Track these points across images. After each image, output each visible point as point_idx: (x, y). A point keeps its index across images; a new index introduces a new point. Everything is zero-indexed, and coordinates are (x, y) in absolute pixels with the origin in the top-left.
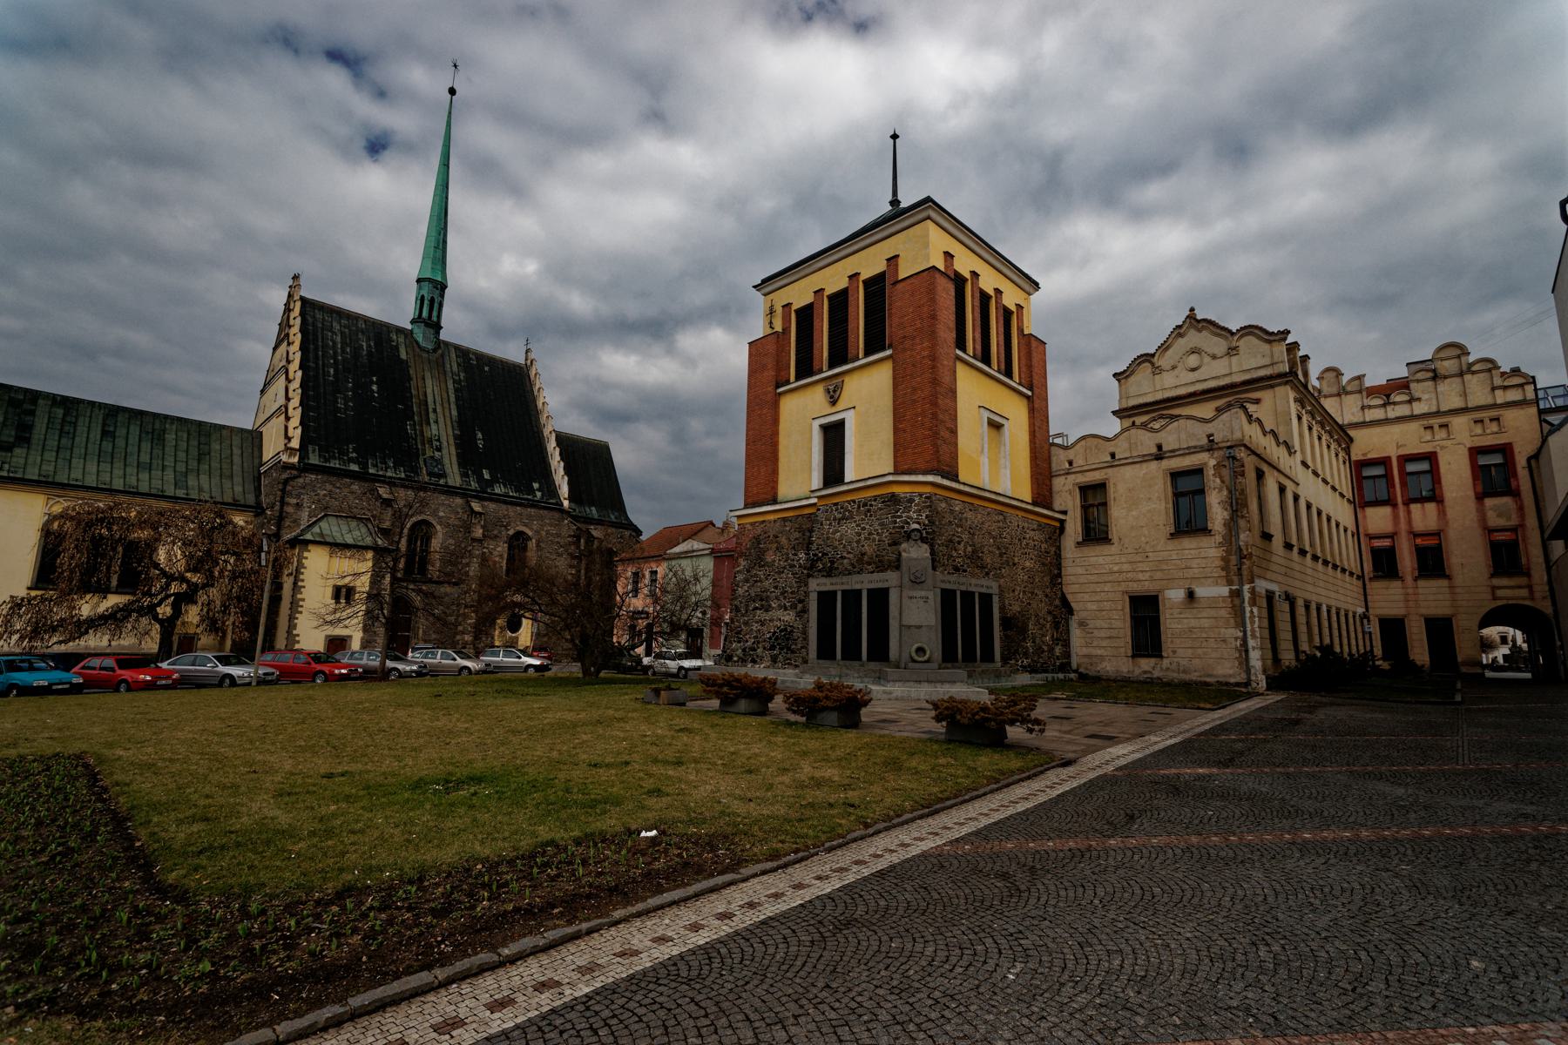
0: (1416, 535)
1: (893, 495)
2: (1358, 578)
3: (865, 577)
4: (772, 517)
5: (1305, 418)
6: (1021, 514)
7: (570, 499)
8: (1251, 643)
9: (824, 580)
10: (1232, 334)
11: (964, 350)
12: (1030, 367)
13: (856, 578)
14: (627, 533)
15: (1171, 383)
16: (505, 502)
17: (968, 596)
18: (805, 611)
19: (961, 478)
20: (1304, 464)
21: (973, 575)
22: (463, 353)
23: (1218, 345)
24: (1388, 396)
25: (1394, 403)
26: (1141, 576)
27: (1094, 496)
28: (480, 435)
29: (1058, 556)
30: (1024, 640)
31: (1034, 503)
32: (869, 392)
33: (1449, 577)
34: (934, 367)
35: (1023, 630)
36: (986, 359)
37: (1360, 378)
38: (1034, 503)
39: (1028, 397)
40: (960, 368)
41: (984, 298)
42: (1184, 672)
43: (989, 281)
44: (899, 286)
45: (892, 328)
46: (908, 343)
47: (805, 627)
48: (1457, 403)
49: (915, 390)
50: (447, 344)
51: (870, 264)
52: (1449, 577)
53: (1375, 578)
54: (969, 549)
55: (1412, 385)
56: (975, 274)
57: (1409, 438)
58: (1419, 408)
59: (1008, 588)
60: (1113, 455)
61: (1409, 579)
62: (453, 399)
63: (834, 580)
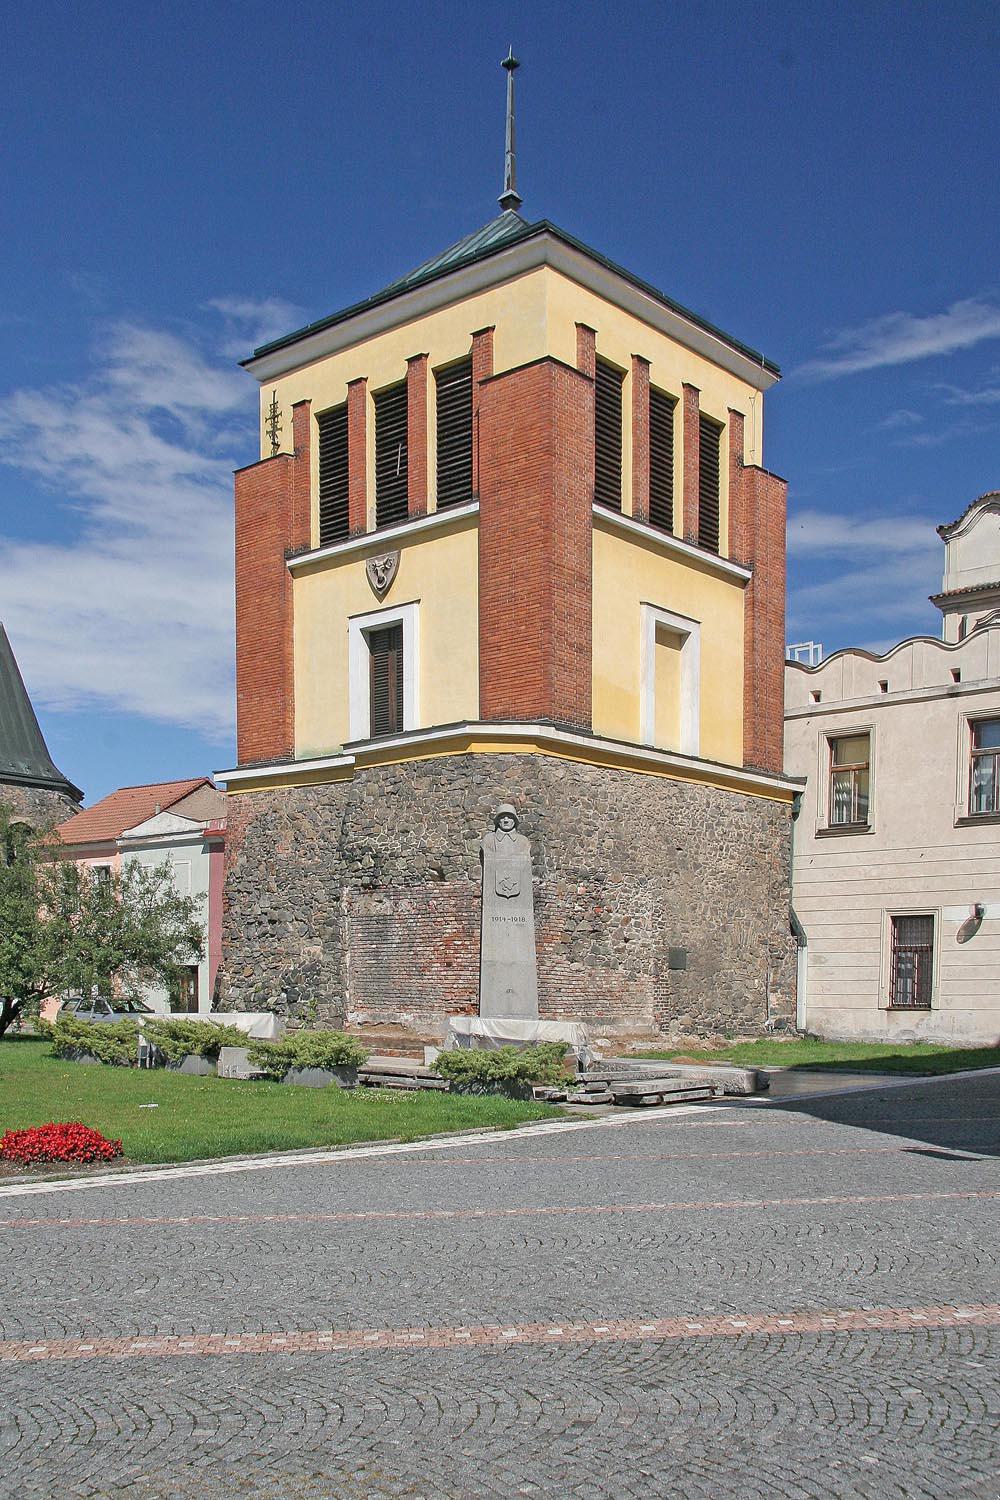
19: (596, 729)
26: (910, 886)
29: (787, 850)
32: (440, 582)
36: (660, 516)
38: (749, 766)
40: (599, 537)
41: (660, 404)
46: (502, 496)
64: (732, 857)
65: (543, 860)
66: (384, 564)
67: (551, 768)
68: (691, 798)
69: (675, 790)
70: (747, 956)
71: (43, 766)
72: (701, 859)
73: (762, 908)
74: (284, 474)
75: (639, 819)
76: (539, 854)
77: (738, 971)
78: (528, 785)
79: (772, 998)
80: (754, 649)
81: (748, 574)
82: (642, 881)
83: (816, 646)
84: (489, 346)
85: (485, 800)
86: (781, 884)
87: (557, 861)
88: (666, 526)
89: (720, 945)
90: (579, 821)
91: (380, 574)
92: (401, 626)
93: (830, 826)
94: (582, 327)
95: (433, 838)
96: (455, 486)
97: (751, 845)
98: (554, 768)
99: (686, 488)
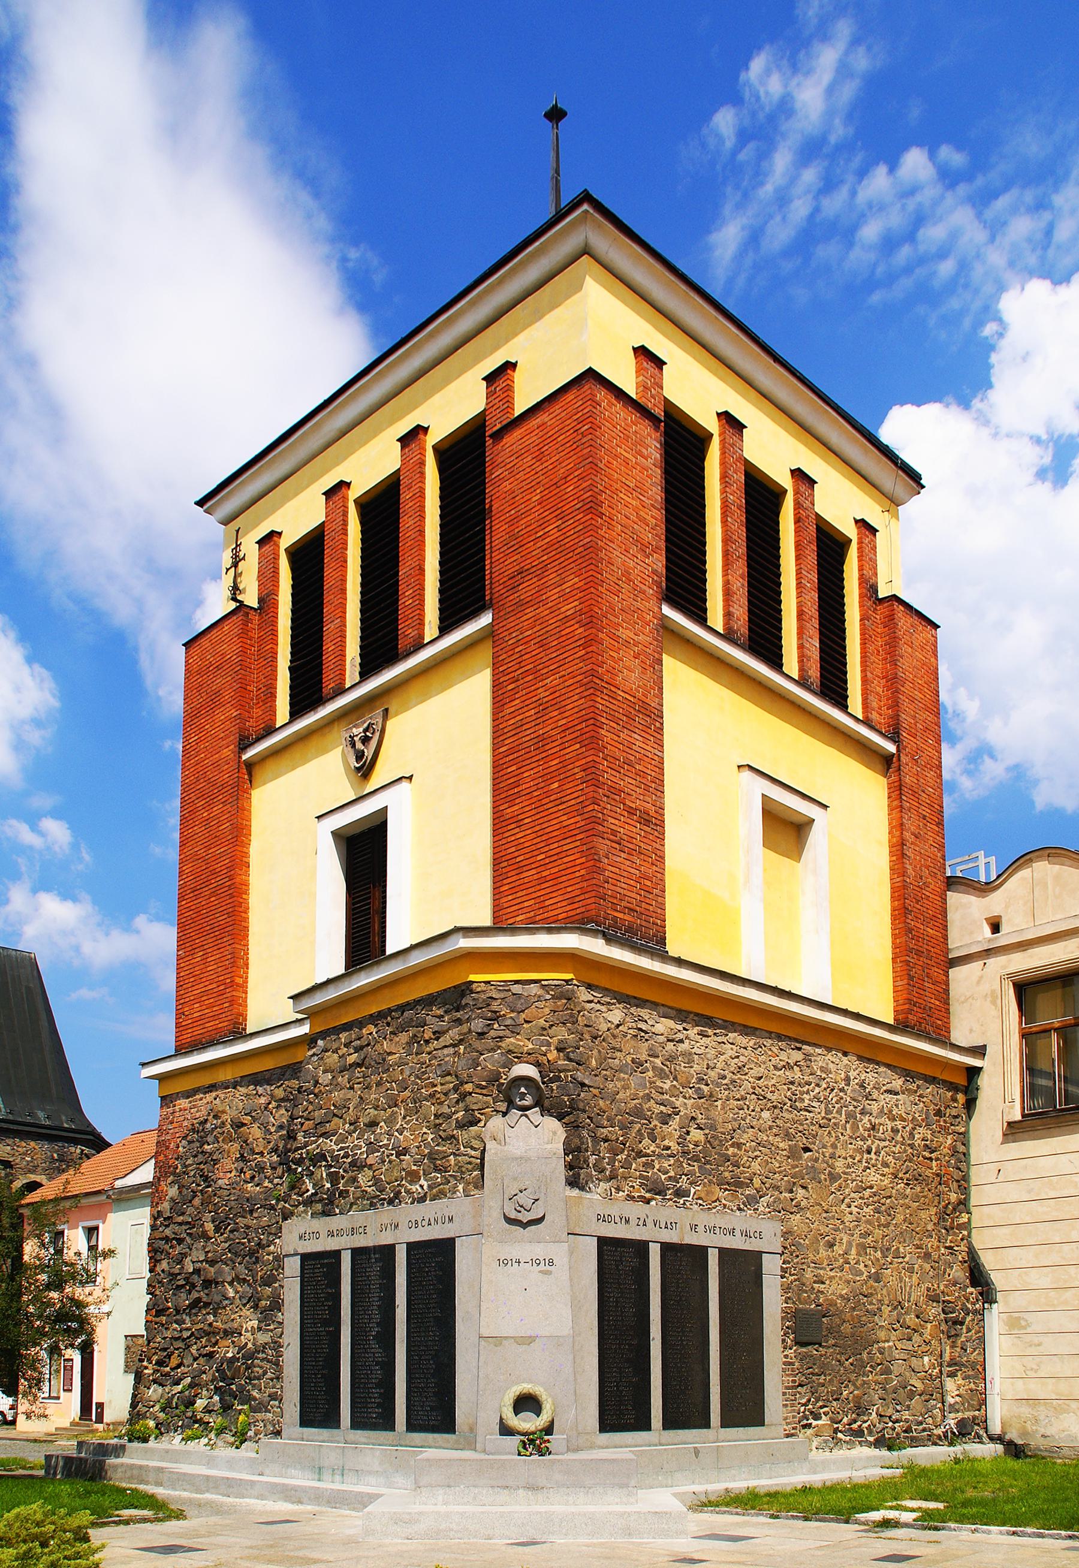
3: (406, 1212)
9: (322, 1224)
12: (893, 681)
13: (386, 1214)
17: (685, 1260)
18: (277, 1305)
21: (708, 1204)
29: (961, 1155)
31: (901, 1026)
32: (440, 750)
34: (590, 641)
35: (859, 1343)
36: (764, 641)
38: (901, 1026)
39: (886, 763)
41: (760, 498)
44: (511, 439)
45: (500, 561)
46: (527, 590)
49: (543, 708)
56: (731, 423)
63: (337, 1222)
64: (886, 1165)
65: (586, 1161)
66: (365, 731)
67: (598, 1006)
68: (822, 1069)
69: (797, 1056)
70: (911, 1319)
71: (67, 1116)
72: (840, 1165)
73: (931, 1243)
74: (244, 632)
75: (744, 1098)
76: (578, 1149)
77: (899, 1345)
78: (561, 1033)
79: (950, 1385)
80: (903, 855)
81: (892, 748)
82: (751, 1201)
83: (987, 860)
85: (490, 1061)
86: (954, 1213)
87: (612, 1162)
89: (871, 1303)
90: (648, 1097)
91: (359, 746)
92: (383, 826)
93: (1023, 1116)
95: (413, 1130)
97: (912, 1146)
98: (604, 1008)
99: (800, 614)
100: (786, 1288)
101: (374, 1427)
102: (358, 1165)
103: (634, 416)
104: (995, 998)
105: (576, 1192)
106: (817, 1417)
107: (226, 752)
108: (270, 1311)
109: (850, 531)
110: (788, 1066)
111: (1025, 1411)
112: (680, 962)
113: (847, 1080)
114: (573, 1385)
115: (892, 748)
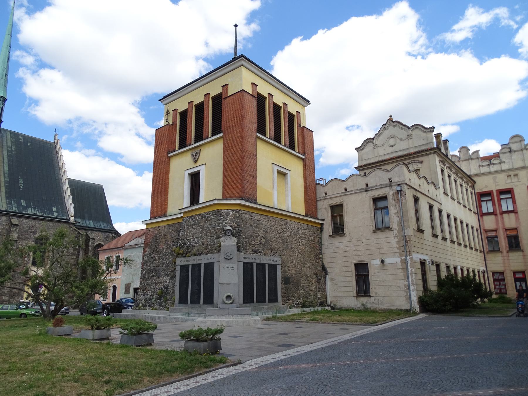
0: (507, 230)
1: (218, 210)
2: (481, 252)
3: (203, 257)
4: (162, 224)
5: (446, 171)
6: (296, 221)
7: (75, 216)
8: (412, 288)
9: (183, 259)
10: (409, 128)
11: (264, 134)
12: (304, 144)
13: (198, 257)
14: (111, 235)
15: (383, 152)
16: (34, 219)
17: (261, 266)
18: (174, 276)
19: (258, 202)
20: (445, 193)
21: (265, 254)
22: (15, 135)
23: (403, 134)
24: (490, 160)
25: (493, 164)
26: (359, 253)
27: (337, 210)
28: (21, 181)
29: (320, 242)
30: (298, 289)
31: (306, 215)
32: (212, 156)
33: (522, 251)
34: (242, 142)
36: (278, 139)
37: (477, 152)
38: (306, 215)
41: (277, 108)
42: (381, 304)
43: (279, 99)
44: (227, 100)
47: (174, 286)
48: (520, 164)
50: (5, 130)
51: (215, 89)
52: (522, 251)
53: (490, 252)
54: (263, 240)
55: (501, 155)
57: (502, 182)
58: (504, 167)
59: (286, 261)
60: (346, 189)
61: (505, 252)
62: (6, 160)
64: (303, 245)
69: (284, 223)
70: (309, 279)
72: (293, 246)
81: (304, 157)
82: (275, 254)
84: (227, 89)
88: (279, 142)
92: (200, 173)
94: (253, 84)
96: (217, 129)
100: (282, 272)
101: (195, 304)
102: (193, 246)
103: (252, 97)
104: (326, 209)
105: (239, 253)
106: (289, 301)
107: (164, 154)
108: (173, 277)
109: (295, 113)
110: (282, 225)
111: (334, 299)
112: (260, 205)
113: (295, 227)
114: (238, 293)
115: (304, 157)
